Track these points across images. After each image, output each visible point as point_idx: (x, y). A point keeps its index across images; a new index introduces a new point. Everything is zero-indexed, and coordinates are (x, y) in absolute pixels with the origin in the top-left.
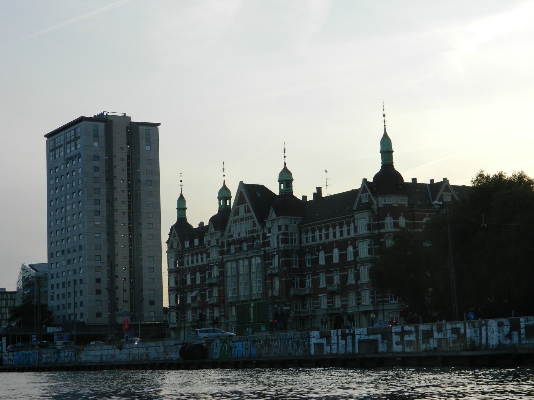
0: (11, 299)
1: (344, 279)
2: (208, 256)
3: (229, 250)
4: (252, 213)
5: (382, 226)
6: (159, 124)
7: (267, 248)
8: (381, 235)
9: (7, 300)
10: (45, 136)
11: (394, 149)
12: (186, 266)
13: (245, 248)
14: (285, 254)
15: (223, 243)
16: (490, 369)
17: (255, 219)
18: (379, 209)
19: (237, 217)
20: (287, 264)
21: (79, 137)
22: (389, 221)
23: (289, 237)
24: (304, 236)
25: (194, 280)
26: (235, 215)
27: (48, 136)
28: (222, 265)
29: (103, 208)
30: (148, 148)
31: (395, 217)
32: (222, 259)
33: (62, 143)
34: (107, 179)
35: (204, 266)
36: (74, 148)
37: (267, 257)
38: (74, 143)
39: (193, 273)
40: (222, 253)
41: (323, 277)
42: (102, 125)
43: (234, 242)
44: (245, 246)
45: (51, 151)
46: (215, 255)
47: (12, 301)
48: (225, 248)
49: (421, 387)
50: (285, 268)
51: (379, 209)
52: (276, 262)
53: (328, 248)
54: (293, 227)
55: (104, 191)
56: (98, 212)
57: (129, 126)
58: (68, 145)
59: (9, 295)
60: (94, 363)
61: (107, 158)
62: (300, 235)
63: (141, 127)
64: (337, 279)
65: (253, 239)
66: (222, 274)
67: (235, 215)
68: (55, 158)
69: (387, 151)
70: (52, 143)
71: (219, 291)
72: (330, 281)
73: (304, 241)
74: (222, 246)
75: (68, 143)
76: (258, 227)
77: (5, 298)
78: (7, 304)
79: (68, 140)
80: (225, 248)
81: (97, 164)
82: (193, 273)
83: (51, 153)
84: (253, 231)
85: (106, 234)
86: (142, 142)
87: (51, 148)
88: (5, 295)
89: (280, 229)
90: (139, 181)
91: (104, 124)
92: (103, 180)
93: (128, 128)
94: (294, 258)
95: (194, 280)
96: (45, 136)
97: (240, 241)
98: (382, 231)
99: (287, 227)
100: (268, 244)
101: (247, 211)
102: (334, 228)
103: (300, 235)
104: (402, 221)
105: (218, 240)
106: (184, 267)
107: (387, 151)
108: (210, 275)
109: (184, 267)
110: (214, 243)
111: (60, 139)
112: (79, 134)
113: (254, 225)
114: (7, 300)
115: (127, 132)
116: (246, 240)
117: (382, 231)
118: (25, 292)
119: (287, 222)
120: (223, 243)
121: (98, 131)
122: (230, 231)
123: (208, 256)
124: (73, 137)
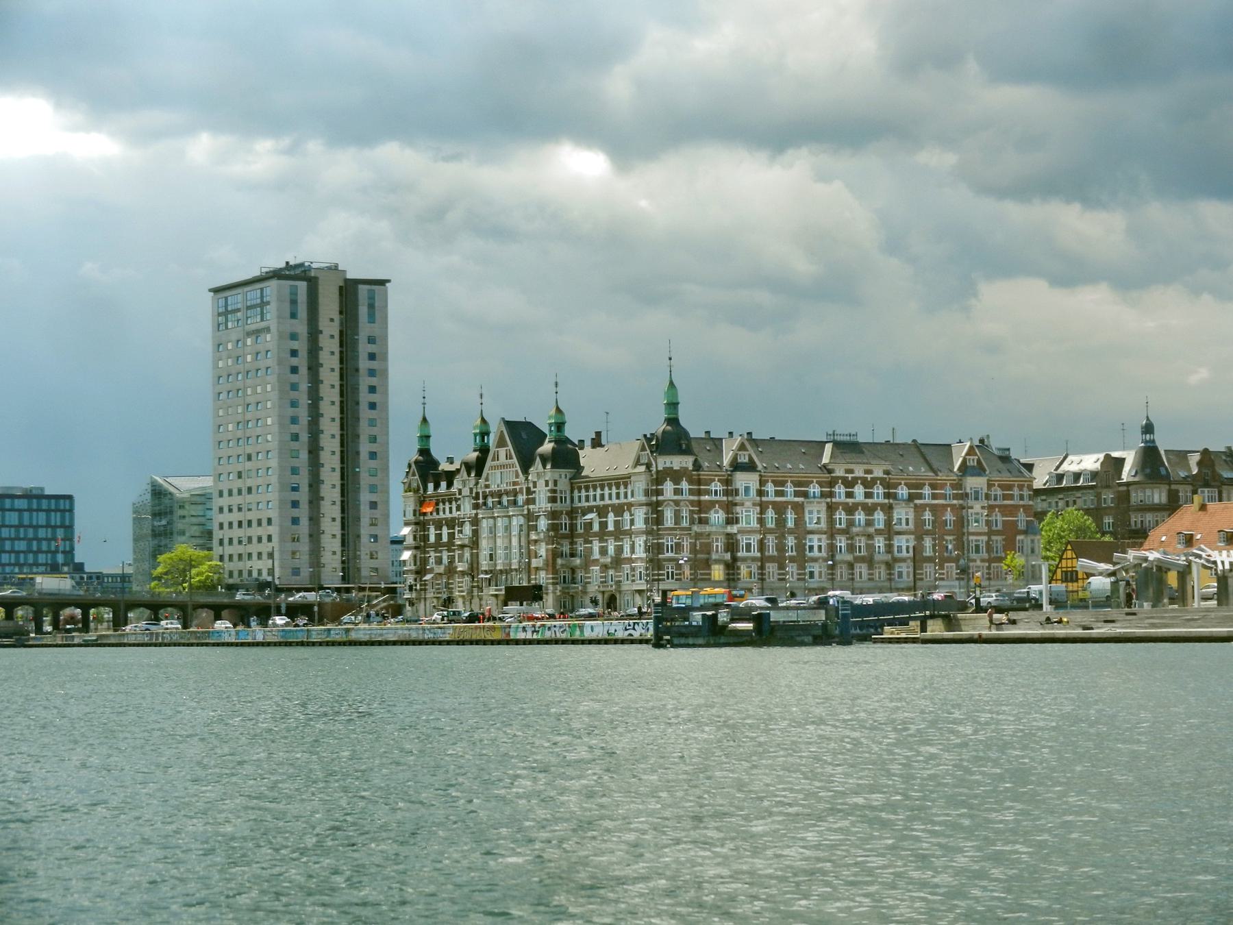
0: (56, 511)
1: (619, 550)
2: (458, 509)
3: (485, 504)
4: (515, 460)
5: (659, 492)
6: (389, 281)
7: (531, 507)
8: (659, 503)
9: (48, 511)
10: (210, 290)
11: (680, 400)
13: (505, 503)
14: (553, 515)
15: (477, 494)
17: (518, 468)
18: (658, 472)
19: (496, 463)
20: (554, 528)
21: (268, 303)
22: (668, 487)
23: (558, 495)
24: (576, 494)
25: (439, 536)
26: (493, 460)
27: (216, 291)
28: (475, 522)
31: (676, 481)
32: (477, 514)
33: (239, 306)
34: (309, 368)
35: (453, 519)
37: (531, 517)
39: (439, 526)
40: (476, 506)
41: (596, 546)
42: (302, 286)
43: (492, 494)
44: (505, 499)
46: (467, 509)
47: (59, 514)
48: (481, 501)
50: (552, 533)
51: (658, 472)
52: (543, 523)
53: (602, 512)
54: (564, 485)
55: (304, 386)
56: (294, 420)
57: (342, 284)
59: (53, 501)
60: (694, 646)
62: (572, 492)
63: (361, 287)
64: (611, 550)
65: (515, 493)
66: (476, 533)
67: (493, 460)
68: (227, 328)
69: (673, 405)
70: (222, 302)
71: (472, 554)
72: (604, 551)
73: (576, 499)
74: (477, 497)
75: (248, 308)
76: (522, 477)
77: (44, 507)
78: (48, 519)
80: (481, 501)
81: (295, 345)
82: (439, 526)
84: (515, 483)
86: (363, 311)
87: (220, 310)
88: (44, 502)
89: (547, 485)
90: (357, 370)
91: (305, 283)
92: (304, 370)
93: (341, 288)
94: (565, 520)
95: (439, 536)
96: (210, 290)
97: (499, 495)
98: (660, 498)
99: (555, 483)
100: (533, 501)
101: (508, 456)
102: (610, 489)
103: (572, 492)
104: (685, 485)
105: (471, 490)
107: (673, 405)
108: (460, 532)
110: (466, 492)
111: (236, 299)
112: (268, 299)
113: (517, 476)
114: (48, 511)
115: (341, 294)
116: (507, 493)
117: (660, 498)
118: (156, 523)
119: (556, 477)
120: (477, 494)
122: (487, 480)
123: (458, 509)
124: (259, 301)
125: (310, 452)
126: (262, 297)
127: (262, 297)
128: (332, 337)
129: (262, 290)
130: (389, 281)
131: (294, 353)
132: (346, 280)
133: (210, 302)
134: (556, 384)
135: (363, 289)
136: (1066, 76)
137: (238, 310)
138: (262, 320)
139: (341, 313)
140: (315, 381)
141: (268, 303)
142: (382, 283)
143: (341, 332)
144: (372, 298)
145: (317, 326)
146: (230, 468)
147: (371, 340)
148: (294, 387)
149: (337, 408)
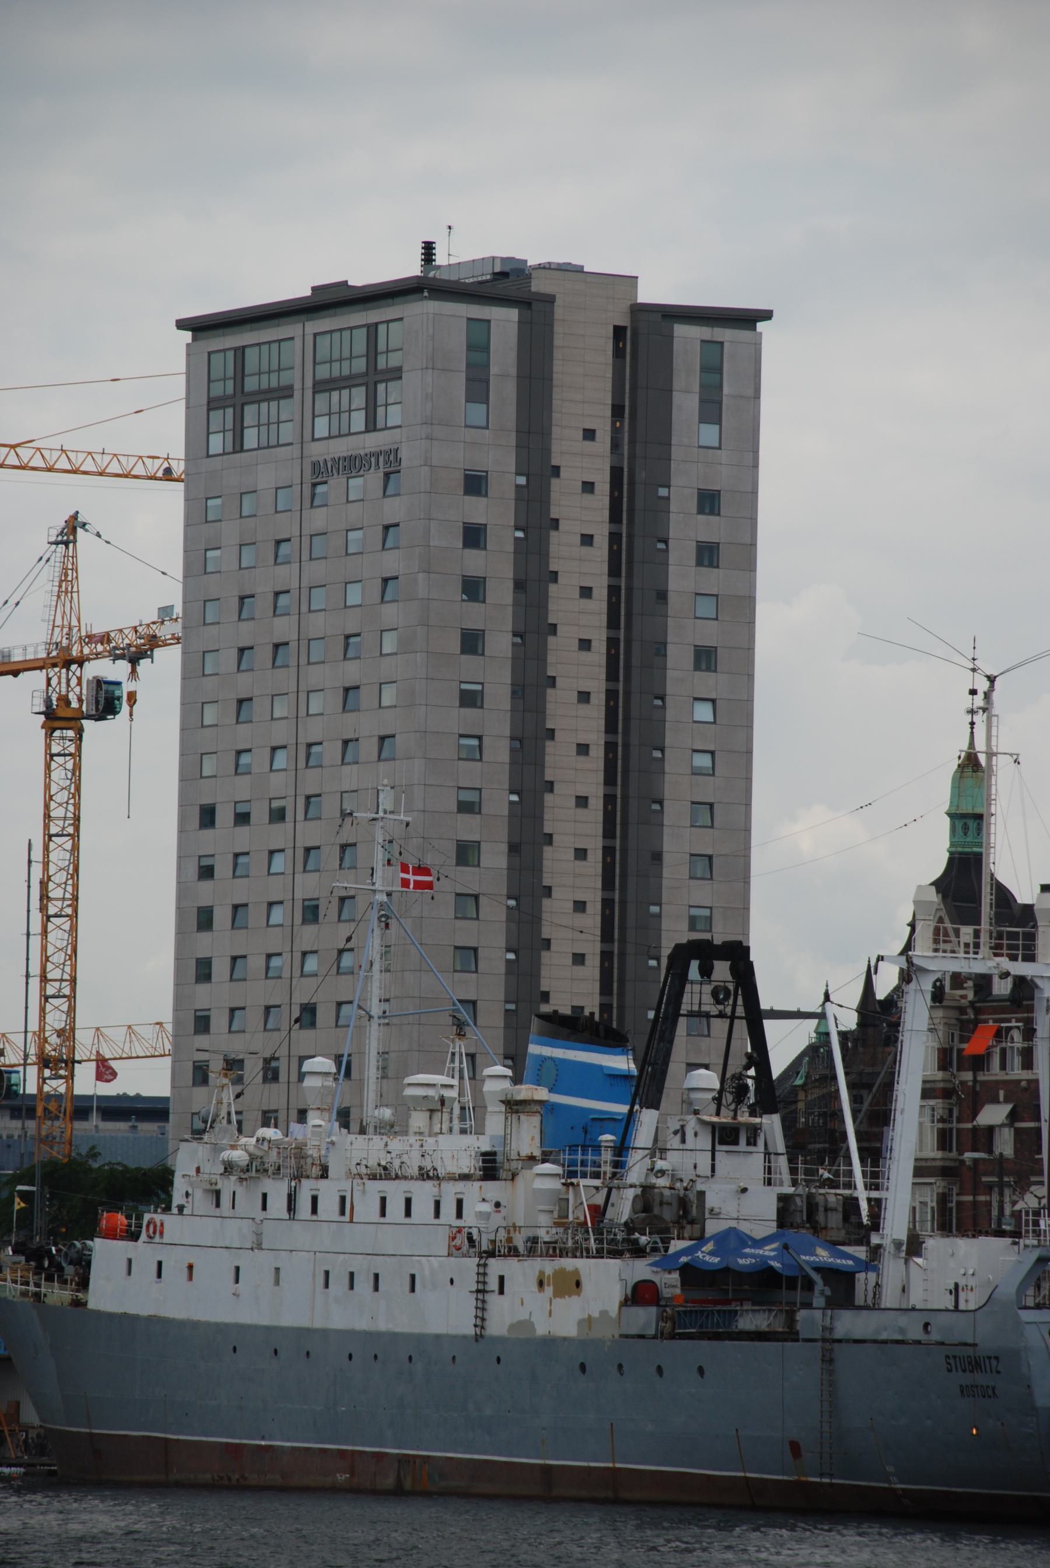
6: (767, 315)
10: (182, 324)
12: (995, 1072)
16: (822, 1523)
21: (396, 374)
27: (200, 327)
29: (496, 720)
30: (709, 434)
36: (358, 421)
38: (359, 396)
42: (505, 320)
45: (213, 404)
49: (700, 827)
57: (624, 321)
58: (322, 399)
61: (522, 480)
63: (683, 331)
68: (239, 447)
75: (321, 386)
79: (323, 372)
81: (476, 509)
83: (216, 416)
85: (504, 848)
86: (686, 403)
87: (218, 390)
90: (662, 596)
93: (619, 332)
96: (182, 324)
106: (982, 1077)
109: (982, 1077)
112: (395, 360)
115: (619, 353)
121: (486, 349)
124: (360, 365)
125: (514, 849)
126: (372, 352)
127: (372, 352)
128: (588, 487)
129: (372, 330)
130: (767, 315)
131: (474, 536)
132: (640, 311)
133: (180, 363)
134: (107, 542)
135: (687, 337)
136: (643, 1212)
137: (285, 392)
138: (371, 426)
139: (617, 411)
140: (533, 631)
141: (396, 374)
142: (748, 319)
143: (616, 474)
144: (712, 368)
145: (546, 451)
146: (276, 890)
147: (709, 502)
148: (472, 642)
149: (596, 712)
